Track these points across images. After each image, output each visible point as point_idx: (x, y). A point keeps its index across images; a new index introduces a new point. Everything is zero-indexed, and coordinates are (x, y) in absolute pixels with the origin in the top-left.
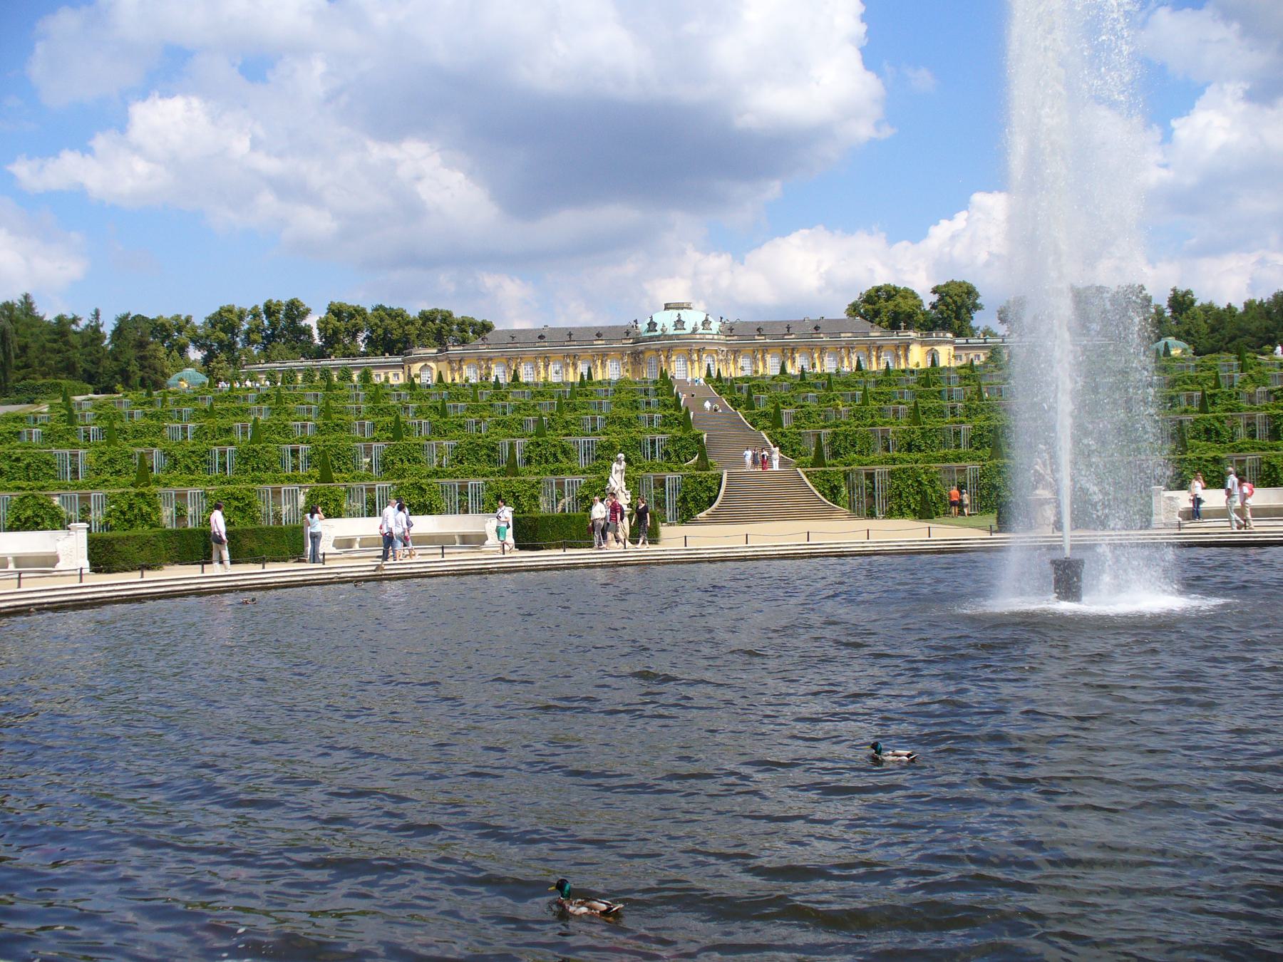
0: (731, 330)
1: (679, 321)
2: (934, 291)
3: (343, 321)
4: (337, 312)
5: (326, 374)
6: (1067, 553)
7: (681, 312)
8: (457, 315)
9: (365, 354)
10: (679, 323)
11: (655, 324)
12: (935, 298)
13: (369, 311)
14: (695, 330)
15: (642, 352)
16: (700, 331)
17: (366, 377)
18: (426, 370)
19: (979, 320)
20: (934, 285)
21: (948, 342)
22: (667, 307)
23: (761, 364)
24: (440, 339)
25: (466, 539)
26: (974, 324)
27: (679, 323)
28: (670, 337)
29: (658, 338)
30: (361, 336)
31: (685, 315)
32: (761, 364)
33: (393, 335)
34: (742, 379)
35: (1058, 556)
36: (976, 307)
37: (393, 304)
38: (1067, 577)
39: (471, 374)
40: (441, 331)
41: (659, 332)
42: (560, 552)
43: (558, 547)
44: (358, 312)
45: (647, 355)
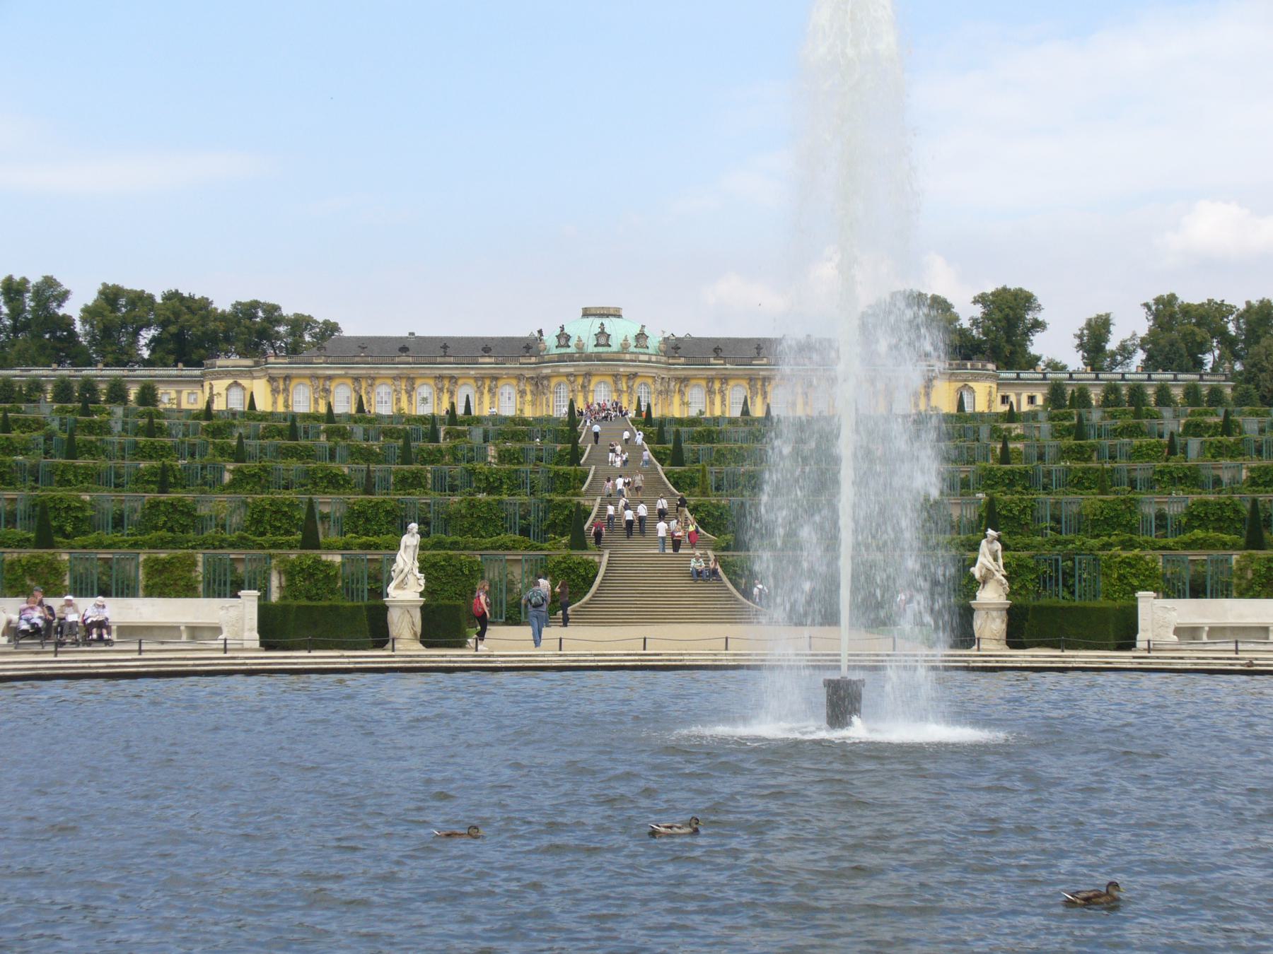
0: (676, 348)
1: (602, 332)
2: (975, 302)
3: (118, 311)
4: (111, 296)
5: (89, 386)
6: (844, 673)
7: (606, 321)
8: (288, 311)
9: (148, 363)
10: (603, 337)
11: (568, 338)
12: (978, 311)
13: (159, 300)
14: (625, 346)
15: (548, 377)
16: (632, 349)
17: (148, 396)
18: (231, 389)
19: (1039, 345)
20: (978, 292)
21: (988, 377)
22: (587, 313)
23: (718, 399)
24: (89, 452)
25: (195, 632)
26: (1033, 350)
27: (603, 337)
28: (589, 358)
29: (571, 358)
30: (146, 335)
31: (611, 325)
32: (718, 399)
33: (194, 334)
34: (680, 422)
35: (834, 676)
36: (1038, 325)
37: (192, 288)
38: (842, 701)
39: (302, 401)
40: (255, 332)
41: (572, 350)
42: (305, 653)
43: (304, 648)
44: (140, 300)
45: (554, 382)
